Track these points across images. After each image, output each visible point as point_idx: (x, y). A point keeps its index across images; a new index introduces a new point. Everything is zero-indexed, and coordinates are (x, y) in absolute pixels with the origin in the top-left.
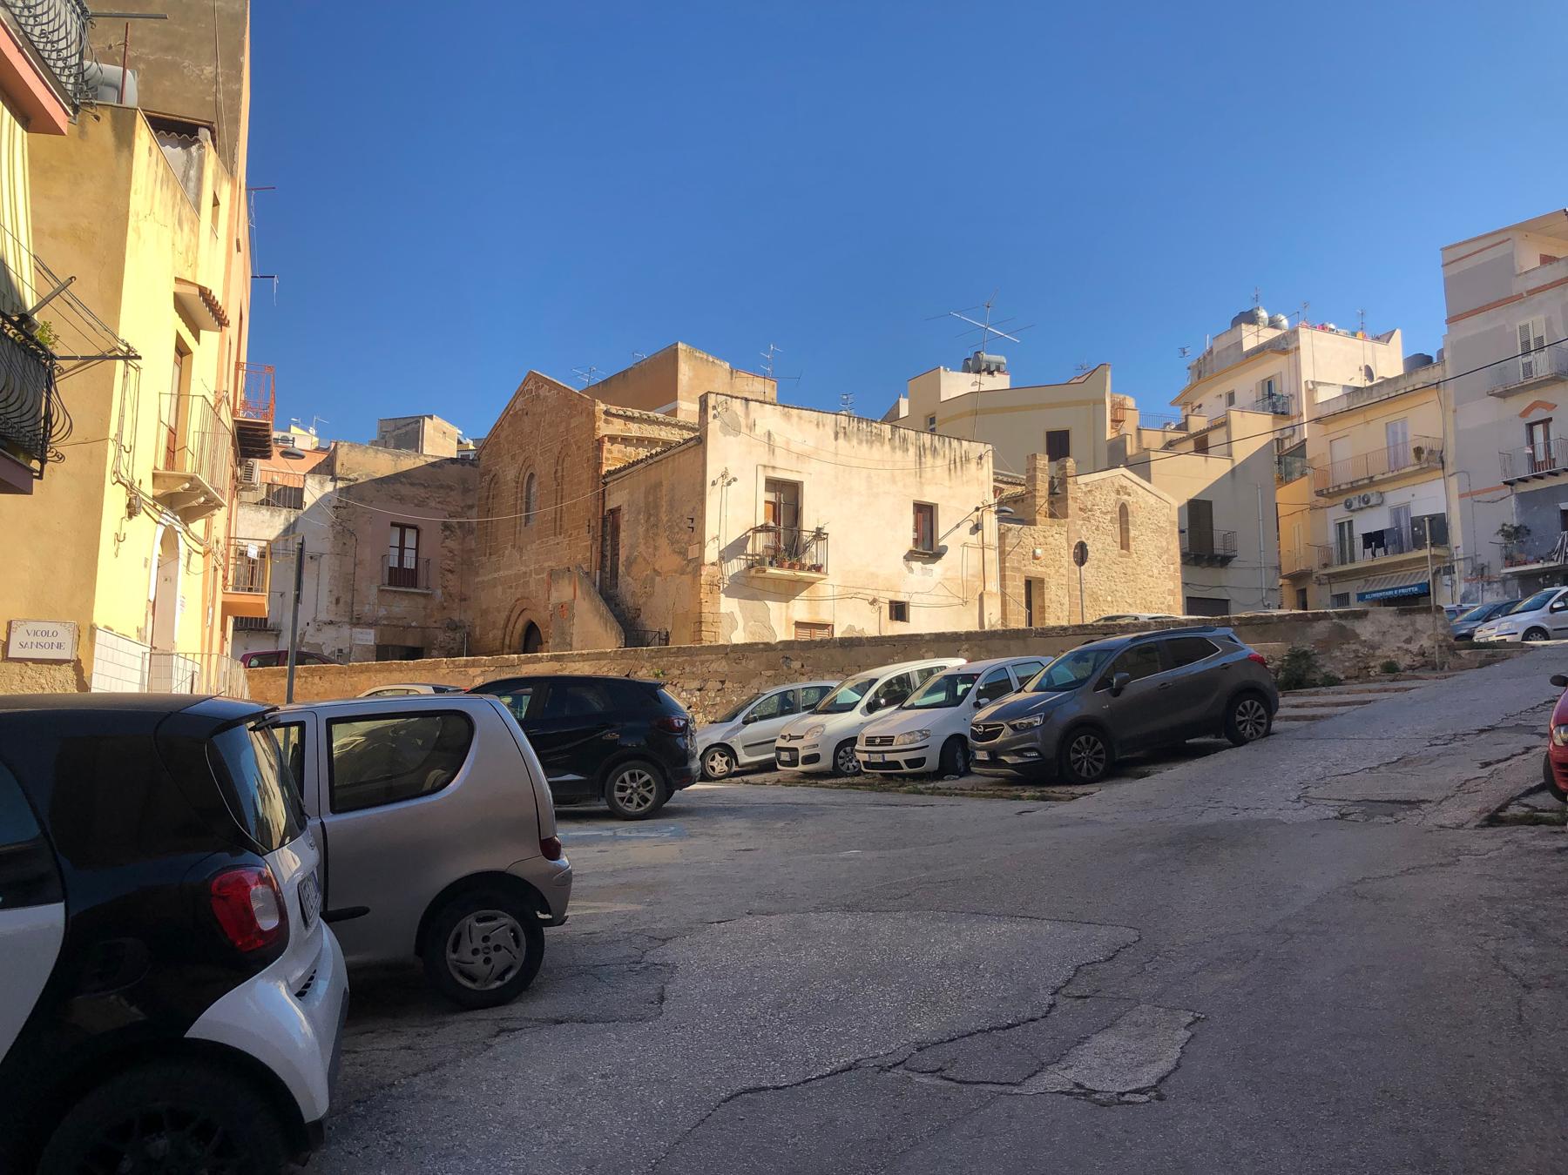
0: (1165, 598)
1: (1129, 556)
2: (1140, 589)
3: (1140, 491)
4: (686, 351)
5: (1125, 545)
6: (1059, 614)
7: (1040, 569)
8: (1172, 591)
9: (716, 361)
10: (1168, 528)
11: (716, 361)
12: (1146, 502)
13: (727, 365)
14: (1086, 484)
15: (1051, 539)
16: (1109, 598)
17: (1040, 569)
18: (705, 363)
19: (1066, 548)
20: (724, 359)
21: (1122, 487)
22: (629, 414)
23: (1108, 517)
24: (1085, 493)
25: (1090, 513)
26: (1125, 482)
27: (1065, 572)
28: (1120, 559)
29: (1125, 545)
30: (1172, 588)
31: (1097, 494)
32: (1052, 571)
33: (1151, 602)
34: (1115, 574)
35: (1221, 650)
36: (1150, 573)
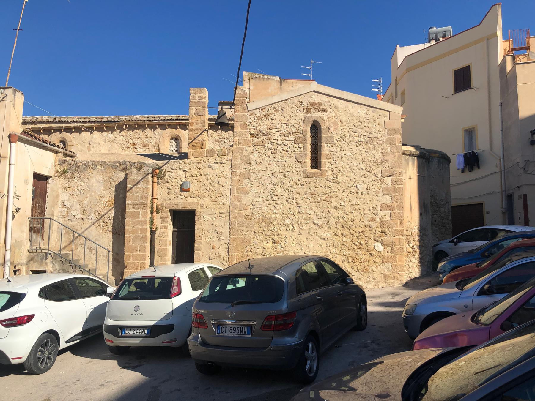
0: (376, 215)
1: (322, 175)
2: (335, 208)
3: (341, 104)
4: (248, 76)
5: (316, 163)
6: (215, 244)
7: (190, 200)
8: (389, 206)
9: (269, 77)
10: (385, 138)
11: (269, 77)
12: (351, 115)
13: (278, 78)
14: (261, 109)
15: (208, 170)
16: (288, 222)
17: (190, 200)
18: (262, 79)
19: (229, 176)
20: (275, 75)
21: (312, 104)
22: (110, 119)
23: (292, 138)
24: (259, 118)
25: (265, 137)
26: (317, 98)
27: (226, 201)
28: (306, 179)
29: (316, 163)
30: (389, 202)
31: (277, 117)
32: (207, 202)
33: (353, 221)
34: (298, 196)
35: (49, 340)
36: (353, 189)
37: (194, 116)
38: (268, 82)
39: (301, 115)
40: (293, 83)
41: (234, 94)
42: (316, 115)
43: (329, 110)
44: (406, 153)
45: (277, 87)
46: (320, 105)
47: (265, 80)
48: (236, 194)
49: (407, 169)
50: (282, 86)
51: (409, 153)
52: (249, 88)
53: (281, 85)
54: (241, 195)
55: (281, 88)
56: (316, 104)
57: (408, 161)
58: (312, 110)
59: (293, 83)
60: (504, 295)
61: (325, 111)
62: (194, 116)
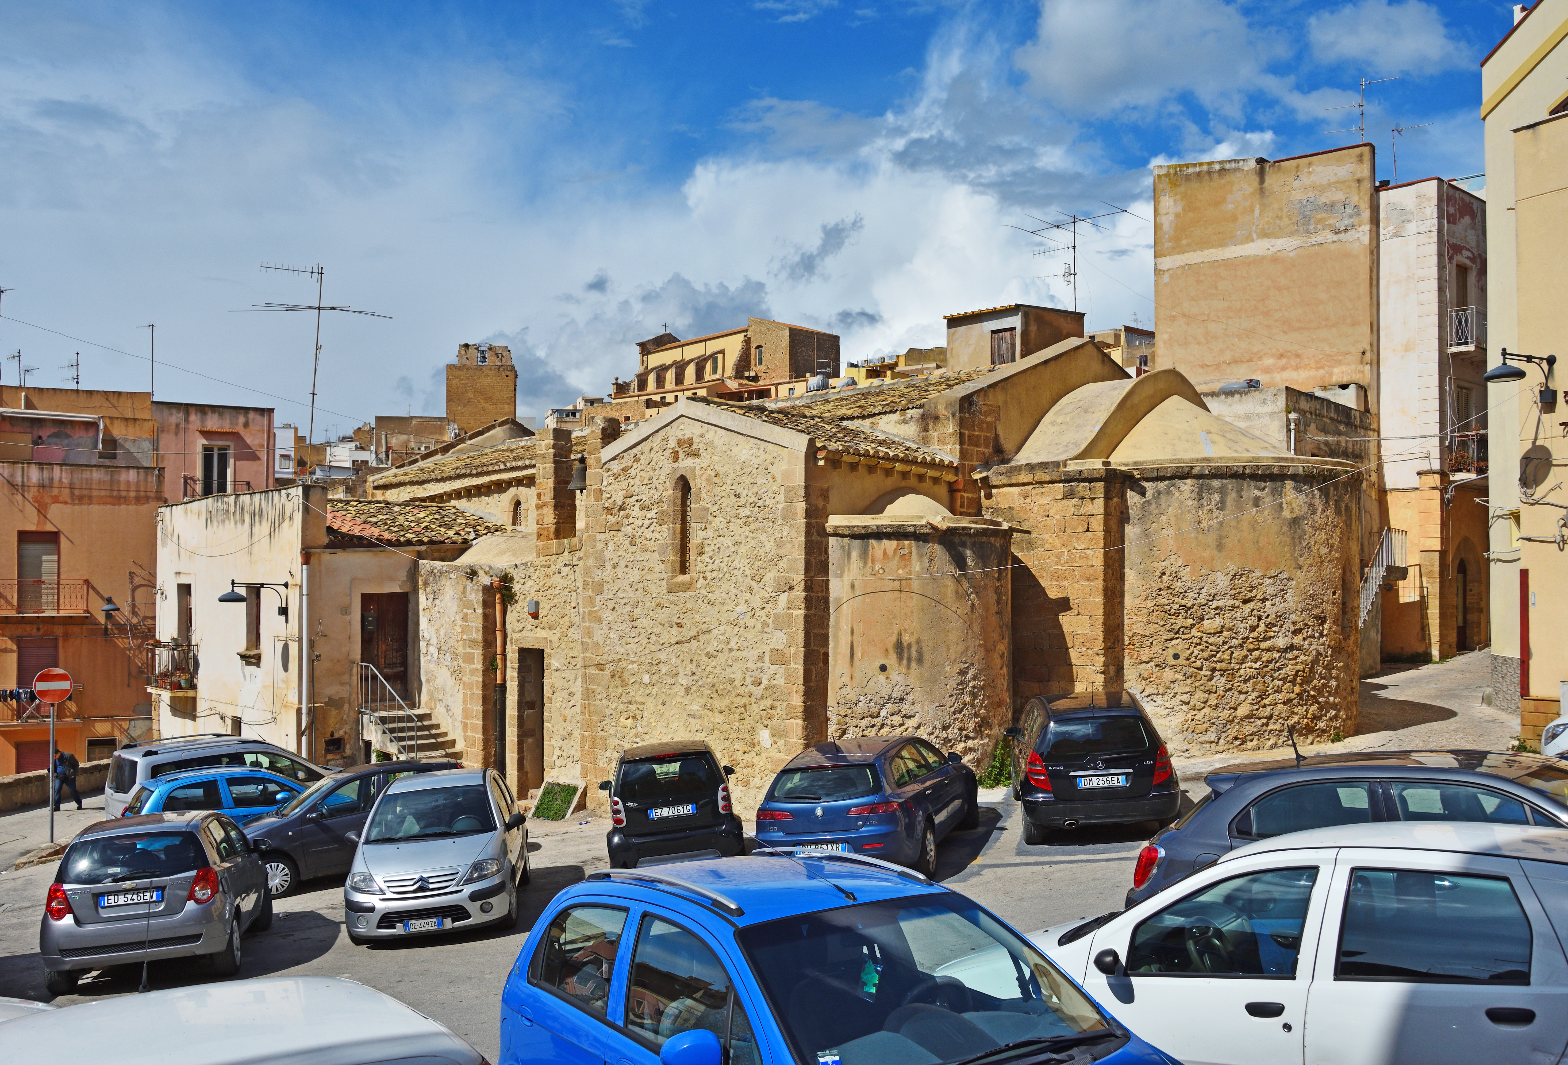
18: (1207, 177)
37: (541, 480)
38: (1223, 181)
39: (668, 466)
40: (1298, 167)
41: (1495, 111)
42: (686, 463)
43: (703, 453)
44: (840, 532)
45: (1251, 190)
46: (691, 444)
47: (1216, 176)
48: (587, 624)
49: (846, 569)
50: (1266, 184)
51: (847, 532)
52: (1074, 247)
53: (1262, 181)
54: (592, 625)
55: (1262, 191)
56: (684, 443)
57: (849, 549)
58: (681, 455)
59: (1298, 167)
60: (1204, 898)
61: (696, 455)
62: (541, 480)
